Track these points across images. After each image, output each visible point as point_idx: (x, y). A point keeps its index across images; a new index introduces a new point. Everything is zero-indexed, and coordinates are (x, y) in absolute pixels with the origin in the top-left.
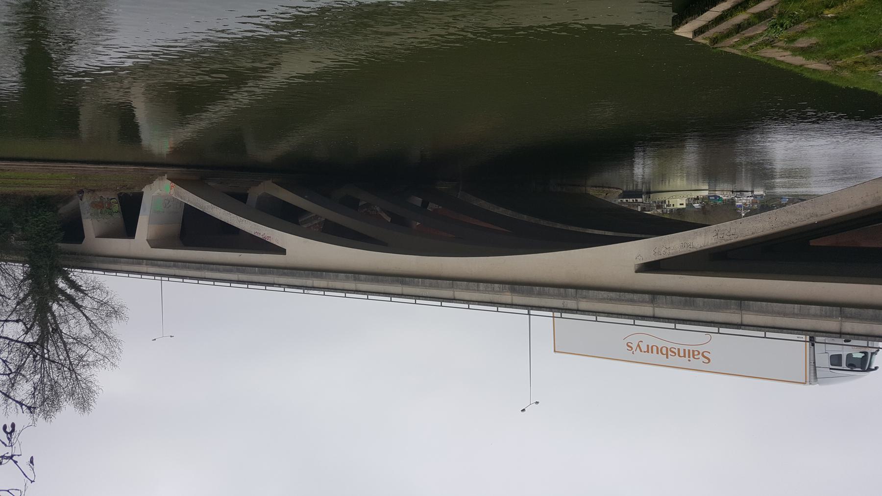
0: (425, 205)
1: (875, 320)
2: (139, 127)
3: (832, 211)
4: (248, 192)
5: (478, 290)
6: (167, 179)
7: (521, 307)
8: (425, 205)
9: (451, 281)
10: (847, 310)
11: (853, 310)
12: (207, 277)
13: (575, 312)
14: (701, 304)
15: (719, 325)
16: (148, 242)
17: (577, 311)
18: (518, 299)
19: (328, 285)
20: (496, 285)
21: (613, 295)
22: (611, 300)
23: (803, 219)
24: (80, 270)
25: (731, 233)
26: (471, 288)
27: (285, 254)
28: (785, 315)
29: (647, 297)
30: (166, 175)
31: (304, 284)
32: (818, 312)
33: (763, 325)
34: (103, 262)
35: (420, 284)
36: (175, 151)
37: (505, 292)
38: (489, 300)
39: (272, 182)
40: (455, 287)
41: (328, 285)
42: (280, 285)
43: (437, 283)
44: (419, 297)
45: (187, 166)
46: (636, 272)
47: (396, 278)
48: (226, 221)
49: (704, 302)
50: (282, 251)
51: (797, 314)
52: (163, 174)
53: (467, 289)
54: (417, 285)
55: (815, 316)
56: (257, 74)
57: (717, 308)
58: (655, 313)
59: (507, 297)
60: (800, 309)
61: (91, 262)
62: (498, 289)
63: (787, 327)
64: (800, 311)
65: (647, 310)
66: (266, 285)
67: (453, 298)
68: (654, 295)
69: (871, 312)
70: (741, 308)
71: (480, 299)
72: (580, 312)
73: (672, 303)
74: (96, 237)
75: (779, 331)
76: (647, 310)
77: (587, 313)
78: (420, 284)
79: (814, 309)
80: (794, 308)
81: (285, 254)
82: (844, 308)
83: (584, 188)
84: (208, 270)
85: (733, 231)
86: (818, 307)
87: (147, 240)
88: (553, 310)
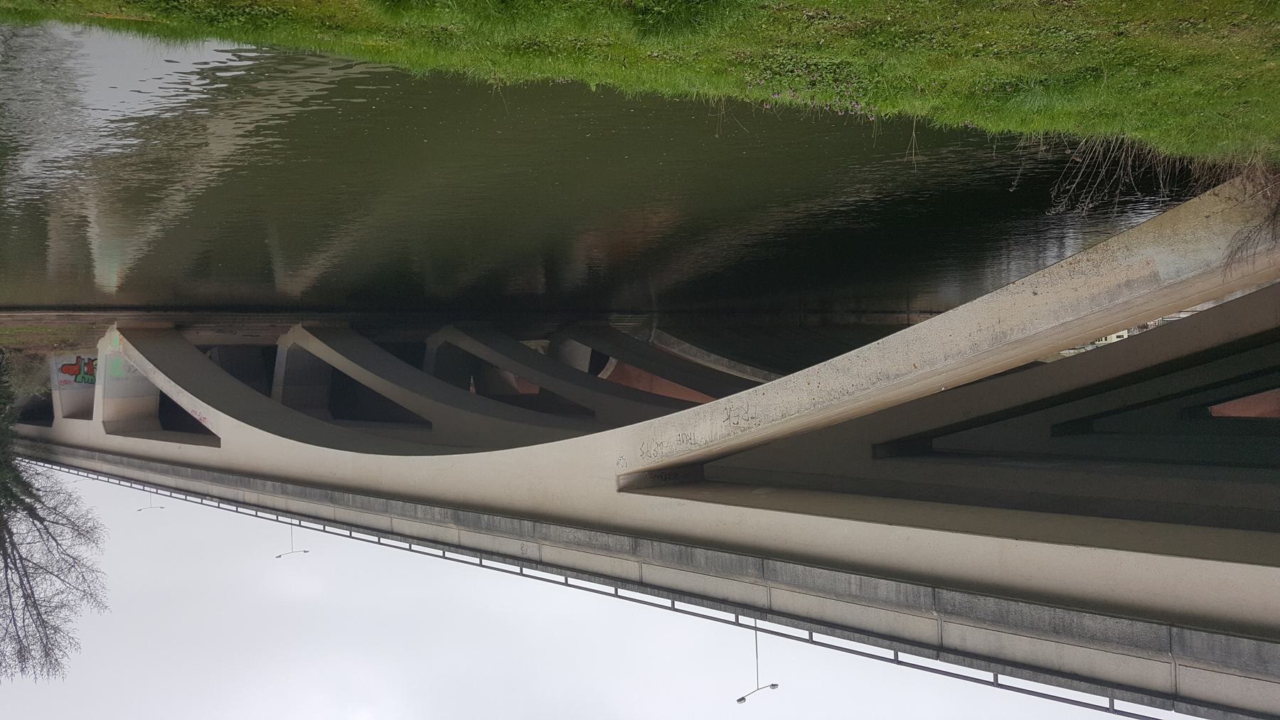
0: (598, 362)
1: (1259, 669)
3: (916, 368)
4: (277, 343)
5: (415, 518)
6: (118, 329)
8: (598, 362)
9: (385, 500)
10: (946, 595)
11: (958, 597)
12: (247, 500)
15: (172, 490)
16: (104, 426)
17: (940, 650)
19: (459, 541)
21: (581, 535)
22: (579, 545)
23: (865, 386)
24: (50, 466)
25: (750, 416)
26: (408, 514)
28: (838, 596)
29: (626, 541)
30: (116, 323)
31: (240, 498)
32: (893, 596)
34: (74, 456)
35: (351, 504)
39: (303, 327)
40: (1176, 648)
45: (147, 308)
46: (620, 490)
47: (323, 492)
49: (707, 558)
50: (210, 438)
51: (856, 597)
52: (111, 321)
53: (1225, 663)
54: (346, 505)
55: (886, 603)
58: (1178, 690)
59: (452, 533)
61: (55, 454)
64: (860, 589)
65: (923, 626)
66: (739, 610)
67: (390, 530)
68: (639, 535)
69: (990, 603)
70: (763, 575)
71: (430, 535)
74: (64, 417)
75: (829, 630)
76: (628, 568)
79: (885, 587)
80: (850, 583)
82: (940, 591)
83: (906, 315)
85: (752, 412)
86: (892, 584)
87: (103, 422)
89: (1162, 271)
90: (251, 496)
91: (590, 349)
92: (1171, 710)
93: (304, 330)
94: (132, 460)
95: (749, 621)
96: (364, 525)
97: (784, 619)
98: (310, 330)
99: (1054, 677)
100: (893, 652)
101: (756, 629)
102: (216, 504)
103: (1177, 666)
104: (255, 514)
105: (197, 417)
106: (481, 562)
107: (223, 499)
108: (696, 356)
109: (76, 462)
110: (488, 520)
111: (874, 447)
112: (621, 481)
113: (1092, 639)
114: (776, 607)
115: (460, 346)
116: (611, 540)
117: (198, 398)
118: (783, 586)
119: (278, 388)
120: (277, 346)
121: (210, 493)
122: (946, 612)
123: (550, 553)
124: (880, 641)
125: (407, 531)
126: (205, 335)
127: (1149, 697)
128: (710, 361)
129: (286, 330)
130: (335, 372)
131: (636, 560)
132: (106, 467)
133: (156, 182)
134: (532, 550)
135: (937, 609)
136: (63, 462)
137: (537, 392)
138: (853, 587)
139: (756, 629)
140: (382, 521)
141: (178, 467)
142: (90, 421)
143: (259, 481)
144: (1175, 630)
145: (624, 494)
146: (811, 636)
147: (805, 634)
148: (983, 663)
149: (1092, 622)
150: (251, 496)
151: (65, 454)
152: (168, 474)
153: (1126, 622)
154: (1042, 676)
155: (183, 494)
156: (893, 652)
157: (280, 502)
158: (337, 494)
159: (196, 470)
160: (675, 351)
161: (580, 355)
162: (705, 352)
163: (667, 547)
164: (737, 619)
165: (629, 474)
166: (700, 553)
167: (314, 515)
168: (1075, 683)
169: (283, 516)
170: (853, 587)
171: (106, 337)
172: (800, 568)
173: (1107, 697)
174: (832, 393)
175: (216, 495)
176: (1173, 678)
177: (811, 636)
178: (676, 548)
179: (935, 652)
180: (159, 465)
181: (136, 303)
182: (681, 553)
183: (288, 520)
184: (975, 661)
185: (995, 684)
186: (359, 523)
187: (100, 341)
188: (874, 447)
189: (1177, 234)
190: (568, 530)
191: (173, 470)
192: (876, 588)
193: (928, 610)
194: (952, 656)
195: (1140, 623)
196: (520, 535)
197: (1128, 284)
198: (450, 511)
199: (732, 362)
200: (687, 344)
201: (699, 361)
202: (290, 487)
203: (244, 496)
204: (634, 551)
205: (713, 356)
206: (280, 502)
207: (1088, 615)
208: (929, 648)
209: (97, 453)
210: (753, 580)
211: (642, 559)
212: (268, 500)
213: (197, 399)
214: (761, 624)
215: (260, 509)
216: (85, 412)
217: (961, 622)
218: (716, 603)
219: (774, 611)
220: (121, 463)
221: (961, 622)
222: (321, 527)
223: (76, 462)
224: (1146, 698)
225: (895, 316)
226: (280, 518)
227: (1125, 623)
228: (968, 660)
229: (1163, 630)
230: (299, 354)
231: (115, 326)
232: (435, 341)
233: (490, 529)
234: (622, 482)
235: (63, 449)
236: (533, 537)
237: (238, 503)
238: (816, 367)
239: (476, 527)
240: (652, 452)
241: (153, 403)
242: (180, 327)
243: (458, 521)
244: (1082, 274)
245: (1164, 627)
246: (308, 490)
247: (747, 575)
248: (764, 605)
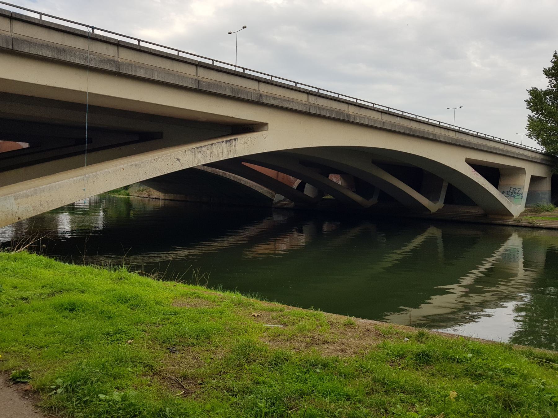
2: (545, 260)
6: (513, 216)
7: (343, 101)
8: (301, 187)
10: (113, 69)
12: (454, 133)
13: (311, 93)
14: (227, 90)
17: (118, 45)
18: (344, 108)
19: (348, 106)
20: (358, 121)
21: (287, 105)
22: (288, 101)
27: (532, 176)
29: (264, 100)
32: (138, 69)
33: (181, 63)
35: (401, 127)
36: (508, 236)
37: (353, 115)
38: (363, 109)
39: (430, 211)
41: (348, 106)
42: (472, 135)
43: (392, 127)
44: (399, 117)
46: (267, 124)
48: (491, 185)
49: (225, 90)
50: (472, 163)
54: (404, 127)
56: (471, 289)
57: (217, 84)
59: (351, 110)
60: (152, 75)
62: (357, 118)
63: (356, 107)
64: (153, 73)
65: (125, 56)
68: (258, 103)
72: (308, 92)
73: (248, 93)
75: (169, 56)
76: (264, 89)
77: (303, 90)
78: (401, 127)
79: (141, 74)
81: (532, 176)
84: (502, 150)
87: (526, 174)
88: (318, 94)
89: (13, 200)
90: (452, 135)
91: (305, 193)
92: (12, 12)
93: (430, 210)
94: (512, 155)
95: (239, 70)
96: (395, 117)
97: (190, 61)
98: (428, 210)
99: (66, 30)
100: (42, 19)
101: (236, 66)
102: (470, 132)
103: (10, 31)
104: (297, 84)
105: (476, 172)
106: (389, 109)
107: (467, 134)
108: (256, 186)
109: (534, 155)
110: (332, 115)
111: (162, 137)
112: (266, 128)
113: (48, 46)
114: (194, 67)
115: (361, 198)
116: (272, 102)
117: (475, 181)
118: (189, 76)
119: (445, 185)
120: (444, 203)
121: (473, 137)
122: (114, 61)
123: (303, 98)
124: (145, 50)
125: (374, 113)
126: (474, 211)
127: (23, 19)
128: (250, 183)
129: (439, 210)
130: (418, 191)
131: (260, 92)
132: (526, 153)
133: (93, 233)
134: (312, 100)
135: (117, 62)
136: (540, 154)
137: (330, 175)
138: (156, 74)
139: (236, 66)
140: (386, 118)
141: (488, 150)
142: (532, 175)
143: (447, 141)
144: (10, 47)
145: (264, 122)
146: (178, 54)
147: (404, 114)
148: (98, 38)
149: (49, 54)
150: (452, 135)
151: (538, 159)
152: (493, 148)
153: (32, 53)
154: (82, 33)
155: (141, 46)
156: (42, 19)
157: (437, 131)
158: (408, 132)
159: (479, 148)
160: (265, 189)
161: (309, 190)
162: (252, 188)
163: (245, 97)
164: (213, 63)
165: (263, 131)
166: (228, 93)
167: (421, 124)
168: (56, 27)
169: (134, 45)
170: (156, 74)
171: (520, 213)
172: (181, 84)
173: (42, 20)
174: (162, 160)
175: (470, 136)
176: (12, 26)
177: (178, 54)
178: (239, 96)
179: (120, 43)
180: (498, 152)
181: (504, 228)
182: (238, 93)
183: (455, 128)
184: (102, 39)
185: (272, 76)
186: (298, 93)
187: (523, 211)
188: (162, 137)
189: (6, 215)
190: (293, 108)
191: (491, 149)
192: (146, 73)
193: (122, 63)
194: (112, 41)
195: (26, 51)
196: (317, 107)
197: (27, 196)
198: (352, 120)
199: (239, 182)
200: (260, 191)
201: (255, 183)
202: (431, 137)
203: (348, 108)
204: (261, 96)
205: (248, 185)
206: (437, 131)
207: (49, 56)
208: (123, 45)
209: (530, 160)
210: (204, 80)
211: (258, 92)
212: (443, 132)
213: (476, 181)
214: (233, 68)
215: (401, 116)
216: (534, 180)
217: (107, 56)
218: (222, 70)
219: (195, 65)
220: (518, 154)
221: (107, 56)
222: (358, 101)
223: (534, 155)
224: (24, 18)
225: (170, 198)
226: (372, 105)
227: (32, 52)
228: (105, 39)
229: (16, 48)
230: (434, 198)
231: (514, 217)
232: (373, 201)
233: (332, 111)
234: (266, 128)
235: (539, 161)
236: (311, 106)
237: (459, 132)
238: (169, 172)
239: (339, 112)
240: (250, 140)
241: (502, 182)
242: (485, 215)
243: (348, 115)
244: (48, 202)
245: (15, 49)
246: (422, 135)
247: (206, 82)
248: (199, 68)
